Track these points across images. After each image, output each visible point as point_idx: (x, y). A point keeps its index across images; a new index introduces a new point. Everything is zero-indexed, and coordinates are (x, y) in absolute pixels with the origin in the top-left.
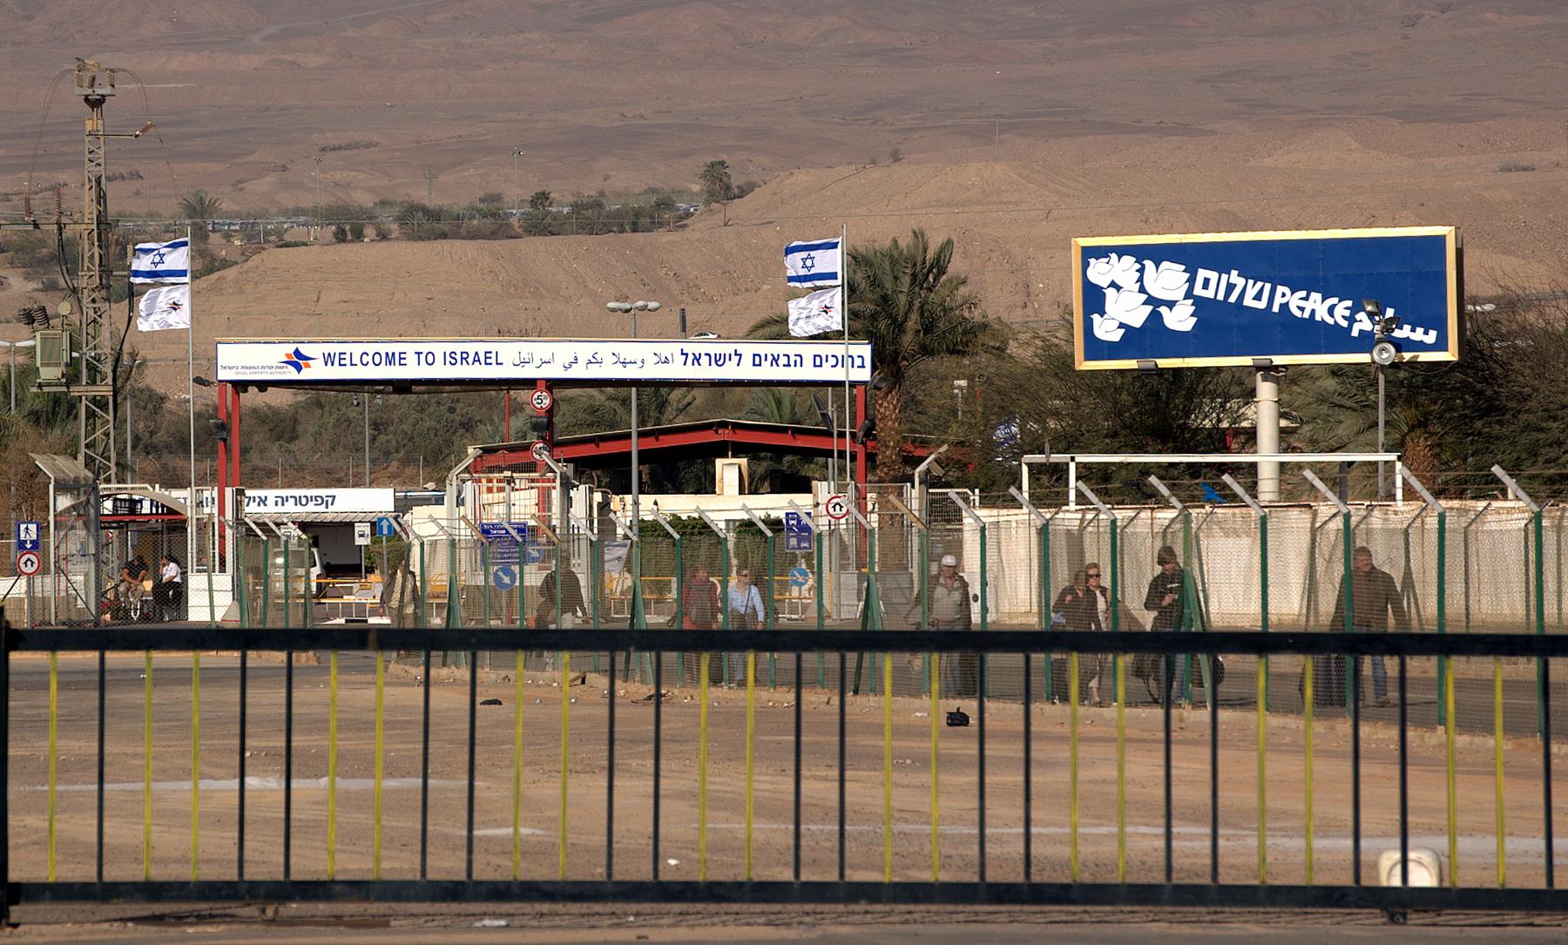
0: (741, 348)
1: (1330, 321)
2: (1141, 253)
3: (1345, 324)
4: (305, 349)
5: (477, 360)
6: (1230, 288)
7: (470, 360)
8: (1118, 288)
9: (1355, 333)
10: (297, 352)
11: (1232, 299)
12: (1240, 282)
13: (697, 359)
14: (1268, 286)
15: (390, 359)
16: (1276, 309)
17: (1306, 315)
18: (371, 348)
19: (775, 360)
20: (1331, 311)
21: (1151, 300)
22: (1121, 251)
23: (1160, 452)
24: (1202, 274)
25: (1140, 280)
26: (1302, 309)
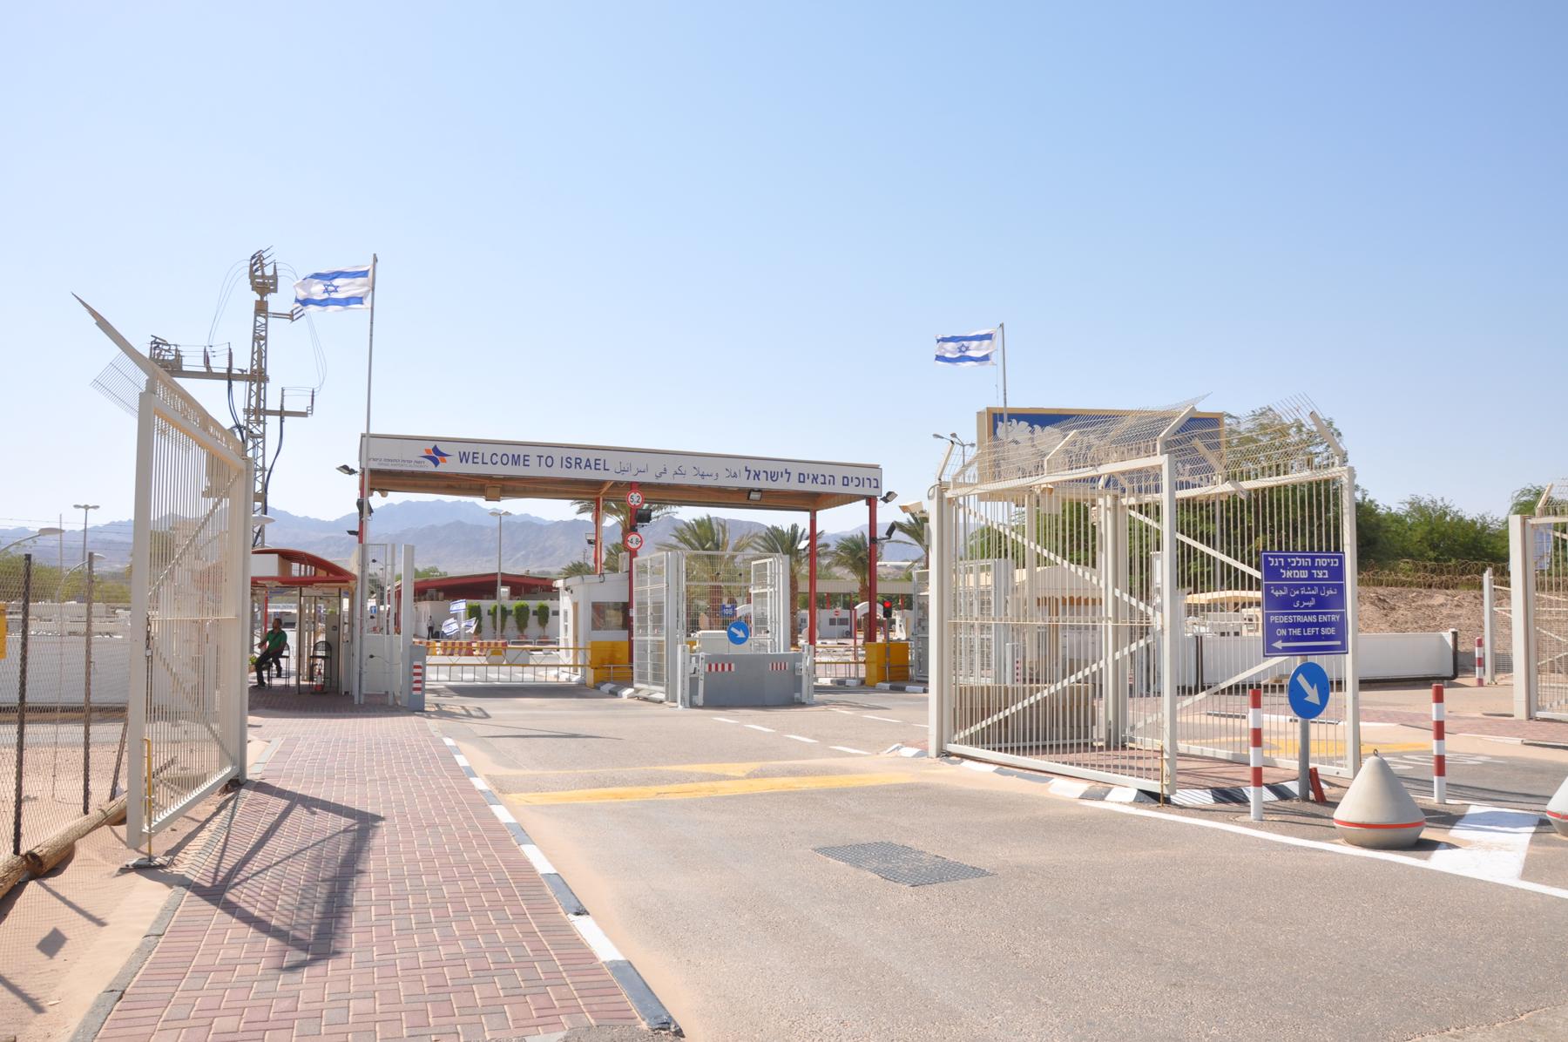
5: (588, 465)
13: (757, 475)
19: (815, 479)
23: (1553, 885)
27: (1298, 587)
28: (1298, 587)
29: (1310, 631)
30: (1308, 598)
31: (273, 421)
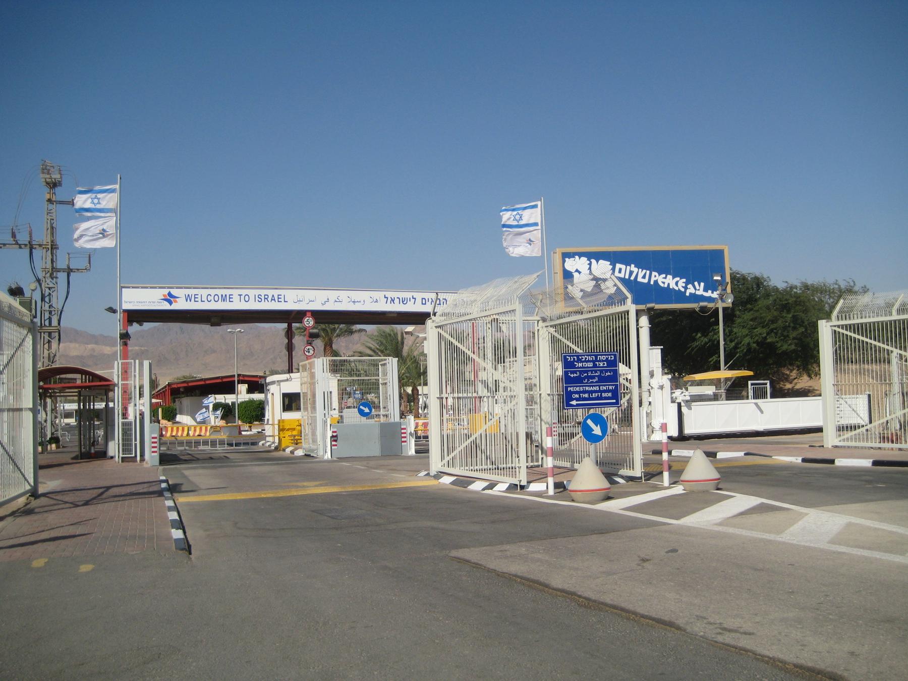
0: (416, 295)
1: (677, 288)
2: (590, 256)
3: (683, 290)
4: (174, 292)
6: (631, 273)
7: (269, 299)
8: (580, 273)
9: (688, 294)
10: (170, 294)
11: (632, 278)
12: (635, 270)
13: (393, 300)
14: (648, 272)
15: (224, 298)
16: (652, 283)
17: (666, 286)
18: (213, 292)
20: (677, 284)
21: (596, 279)
22: (581, 255)
24: (618, 266)
25: (590, 268)
26: (664, 283)
27: (587, 372)
28: (587, 372)
29: (594, 395)
30: (593, 377)
31: (62, 276)
